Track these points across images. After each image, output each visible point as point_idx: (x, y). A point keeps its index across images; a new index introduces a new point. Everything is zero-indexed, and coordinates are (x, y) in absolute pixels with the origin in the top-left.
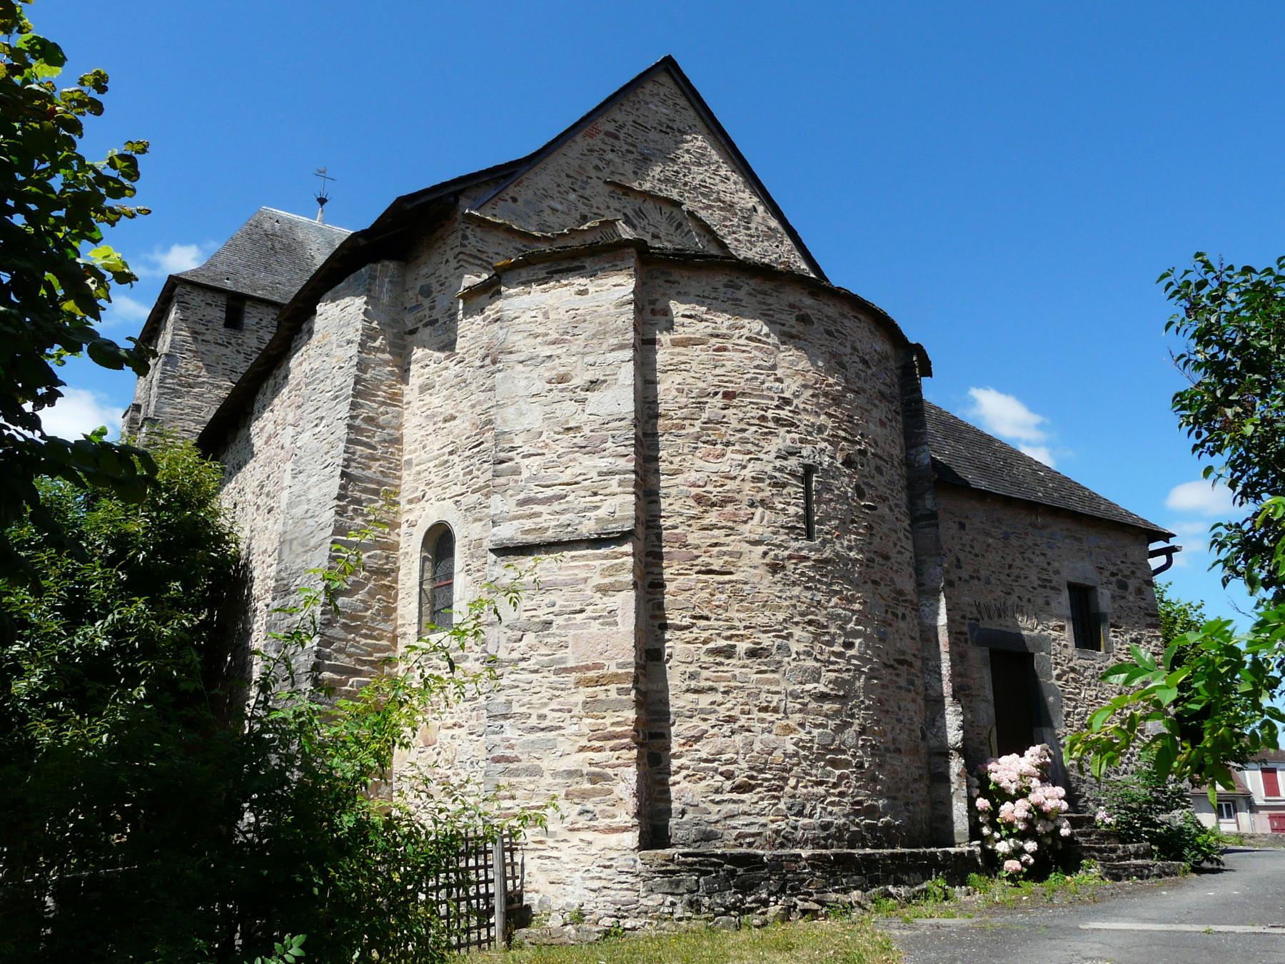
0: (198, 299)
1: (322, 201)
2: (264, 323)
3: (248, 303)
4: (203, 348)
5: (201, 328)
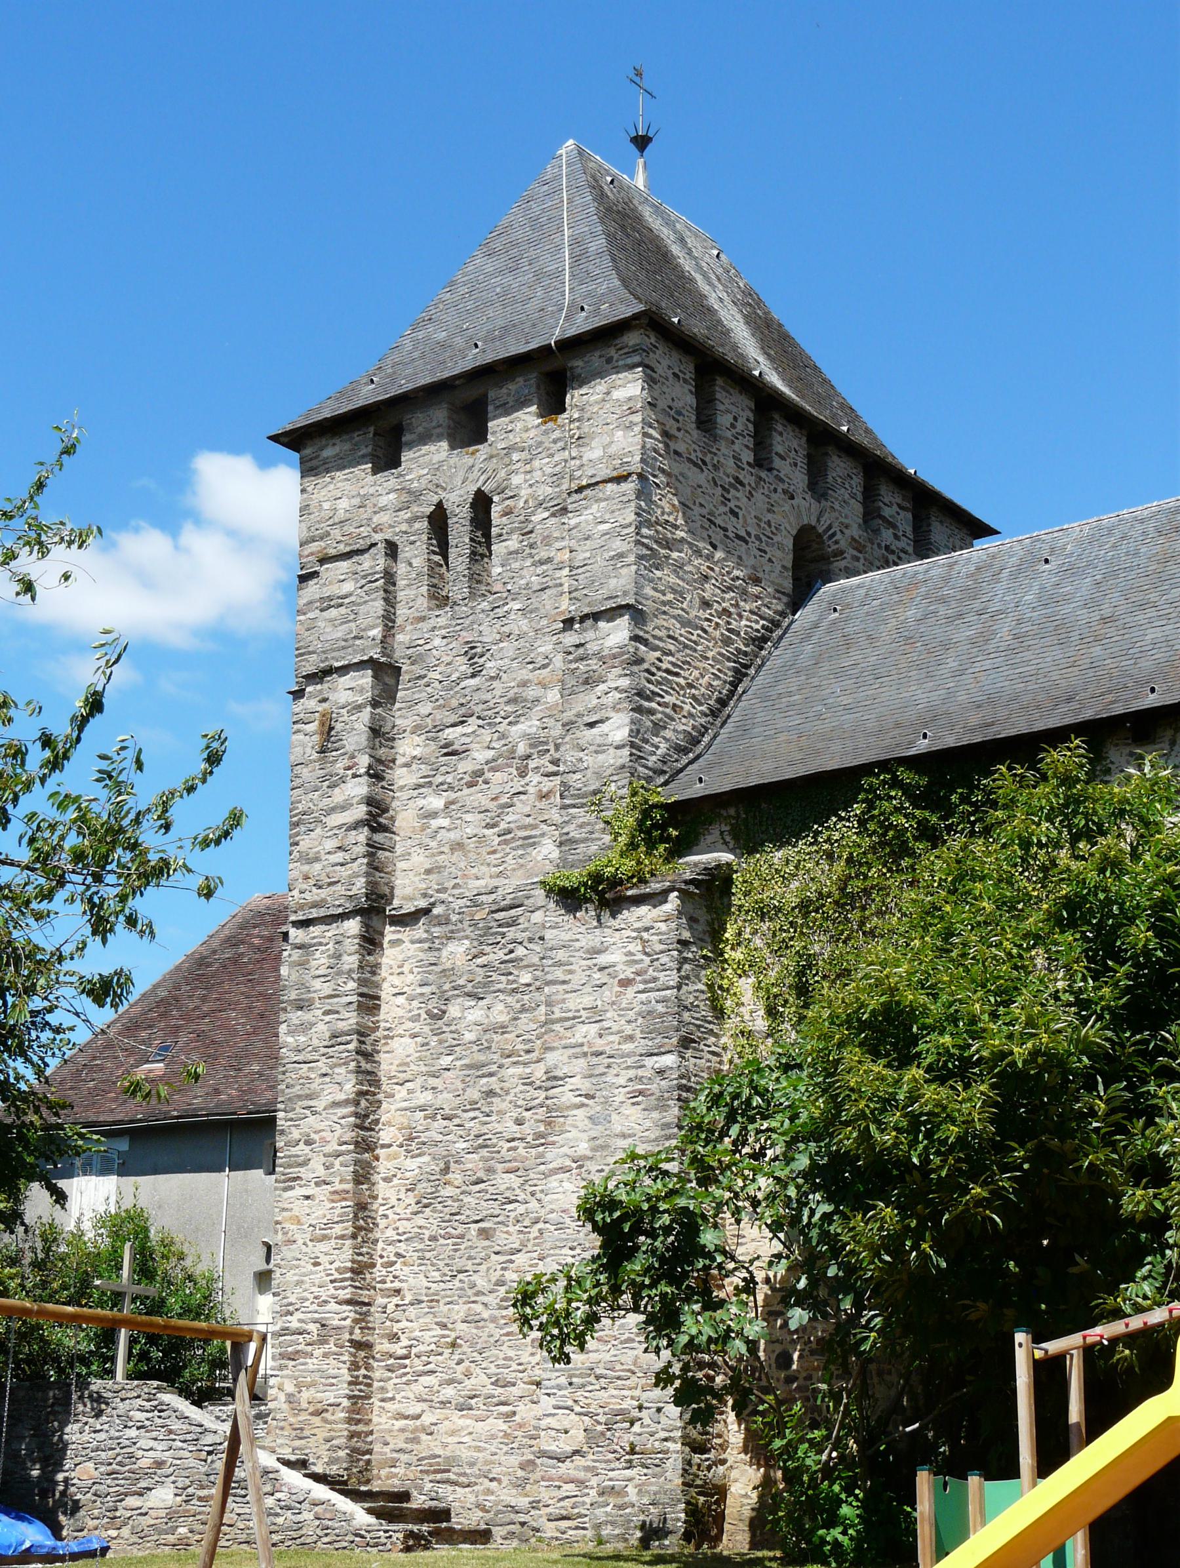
0: (665, 362)
1: (641, 142)
2: (740, 426)
3: (720, 381)
4: (677, 468)
5: (671, 426)
